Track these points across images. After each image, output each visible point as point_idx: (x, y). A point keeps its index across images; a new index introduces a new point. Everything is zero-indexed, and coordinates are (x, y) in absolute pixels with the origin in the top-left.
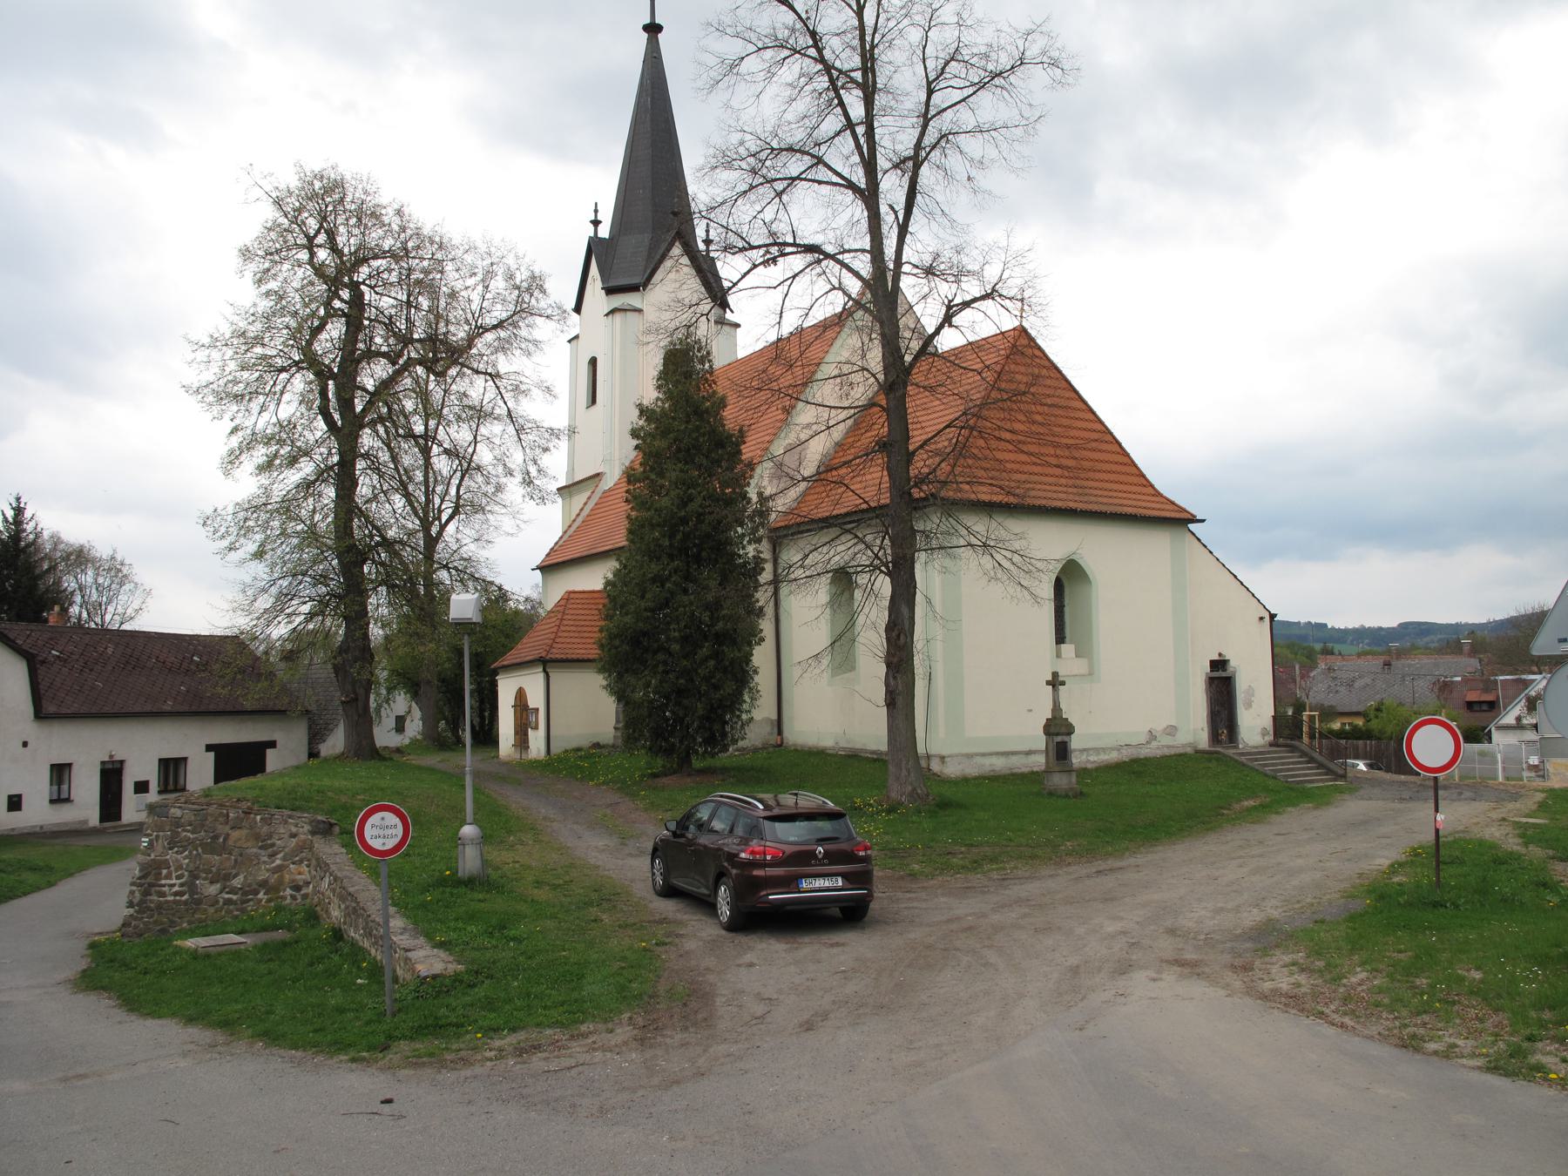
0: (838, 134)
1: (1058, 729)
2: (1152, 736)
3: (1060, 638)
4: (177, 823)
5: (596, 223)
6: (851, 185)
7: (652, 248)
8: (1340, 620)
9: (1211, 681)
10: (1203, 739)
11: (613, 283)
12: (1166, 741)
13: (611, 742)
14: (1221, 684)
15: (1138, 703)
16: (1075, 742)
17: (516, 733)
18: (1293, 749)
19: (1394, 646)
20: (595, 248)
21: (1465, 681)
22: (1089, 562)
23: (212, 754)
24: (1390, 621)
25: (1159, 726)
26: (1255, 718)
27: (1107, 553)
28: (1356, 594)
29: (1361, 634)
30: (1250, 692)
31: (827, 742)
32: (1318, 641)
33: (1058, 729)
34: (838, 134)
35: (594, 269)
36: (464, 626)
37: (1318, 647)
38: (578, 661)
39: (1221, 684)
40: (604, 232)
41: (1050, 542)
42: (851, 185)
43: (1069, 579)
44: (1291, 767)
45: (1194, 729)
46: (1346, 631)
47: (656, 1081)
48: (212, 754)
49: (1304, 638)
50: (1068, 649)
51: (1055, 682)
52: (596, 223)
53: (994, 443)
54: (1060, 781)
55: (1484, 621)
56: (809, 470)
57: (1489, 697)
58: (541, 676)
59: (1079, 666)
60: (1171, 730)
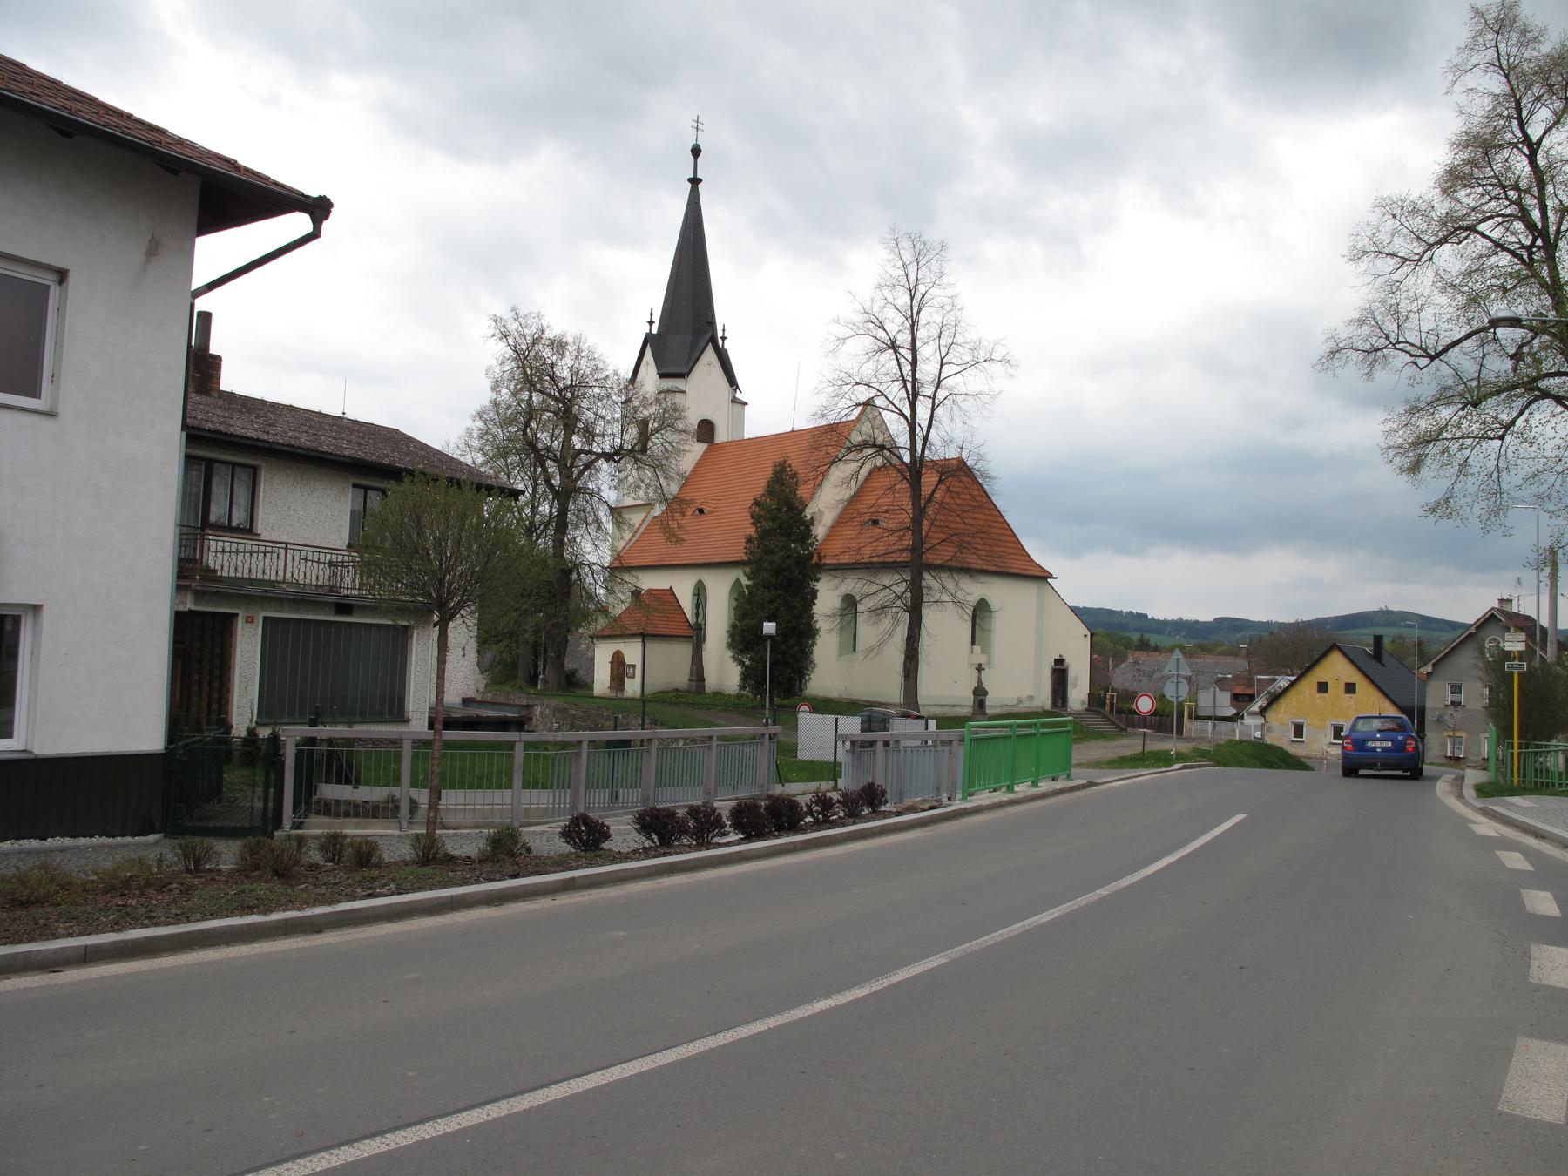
1: (980, 692)
2: (1020, 701)
3: (973, 643)
4: (574, 717)
5: (651, 323)
6: (902, 414)
7: (693, 348)
8: (1161, 610)
9: (1054, 671)
11: (663, 371)
12: (1027, 704)
13: (685, 687)
14: (1060, 674)
15: (1018, 682)
17: (612, 679)
18: (1098, 713)
19: (1206, 639)
20: (648, 340)
21: (1235, 678)
22: (994, 603)
24: (1206, 615)
25: (1024, 695)
26: (1078, 694)
28: (1177, 587)
29: (1179, 626)
30: (1076, 679)
31: (834, 695)
32: (1136, 630)
33: (980, 692)
35: (649, 355)
36: (770, 637)
37: (1135, 637)
39: (1060, 674)
40: (655, 331)
41: (974, 590)
42: (902, 414)
43: (980, 611)
44: (1096, 722)
45: (1043, 697)
46: (1165, 623)
49: (1124, 627)
50: (977, 648)
52: (651, 323)
53: (944, 521)
55: (1292, 620)
56: (828, 596)
57: (1249, 691)
58: (640, 645)
60: (1031, 698)
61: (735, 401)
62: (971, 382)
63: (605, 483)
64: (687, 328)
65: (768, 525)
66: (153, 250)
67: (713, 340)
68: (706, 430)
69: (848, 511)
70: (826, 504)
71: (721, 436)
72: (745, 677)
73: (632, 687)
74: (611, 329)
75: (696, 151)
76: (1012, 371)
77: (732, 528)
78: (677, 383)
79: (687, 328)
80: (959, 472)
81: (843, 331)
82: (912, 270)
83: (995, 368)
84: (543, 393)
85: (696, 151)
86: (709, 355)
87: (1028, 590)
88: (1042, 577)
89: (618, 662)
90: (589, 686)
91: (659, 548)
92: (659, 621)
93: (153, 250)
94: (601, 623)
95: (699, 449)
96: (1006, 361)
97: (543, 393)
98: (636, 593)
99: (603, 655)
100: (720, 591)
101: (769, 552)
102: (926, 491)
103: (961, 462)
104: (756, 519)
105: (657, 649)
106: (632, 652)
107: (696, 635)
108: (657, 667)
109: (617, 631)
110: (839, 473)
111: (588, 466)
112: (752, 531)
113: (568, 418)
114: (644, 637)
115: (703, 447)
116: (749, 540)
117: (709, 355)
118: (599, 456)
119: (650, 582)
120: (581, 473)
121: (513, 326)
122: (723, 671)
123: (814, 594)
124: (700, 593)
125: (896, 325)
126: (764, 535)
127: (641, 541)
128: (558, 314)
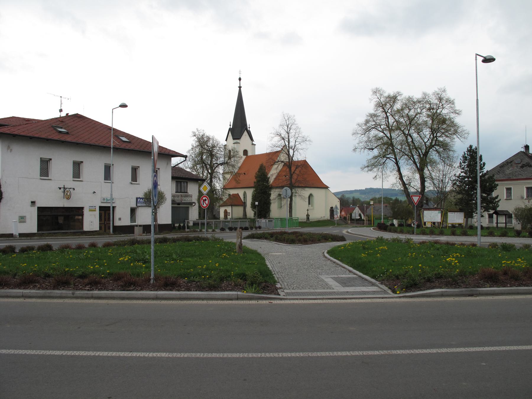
0: (112, 195)
1: (308, 216)
3: (309, 204)
10: (329, 218)
15: (320, 212)
16: (310, 218)
20: (230, 130)
23: (523, 150)
26: (337, 216)
27: (315, 192)
33: (308, 216)
34: (112, 195)
35: (230, 134)
38: (48, 140)
39: (332, 211)
43: (311, 196)
47: (175, 161)
48: (523, 150)
51: (308, 210)
54: (308, 222)
56: (274, 194)
59: (312, 208)
60: (324, 217)
61: (253, 144)
62: (303, 145)
63: (220, 170)
64: (239, 127)
65: (259, 179)
66: (167, 164)
67: (246, 129)
68: (245, 152)
69: (279, 175)
70: (273, 173)
71: (250, 154)
72: (255, 214)
73: (229, 217)
74: (219, 134)
75: (240, 79)
76: (311, 143)
77: (251, 178)
78: (238, 141)
79: (239, 127)
80: (304, 164)
81: (273, 136)
82: (287, 121)
83: (308, 142)
84: (205, 148)
85: (240, 79)
86: (246, 133)
87: (323, 191)
88: (326, 187)
89: (226, 212)
90: (219, 218)
91: (234, 184)
92: (235, 201)
93: (167, 164)
94: (221, 202)
95: (244, 157)
96: (309, 141)
97: (205, 148)
98: (230, 195)
99: (222, 210)
100: (250, 193)
101: (259, 185)
102: (293, 171)
103: (305, 162)
104: (256, 177)
105: (235, 208)
106: (229, 209)
107: (244, 205)
108: (237, 212)
109: (225, 205)
110: (275, 166)
111: (217, 166)
112: (255, 180)
113: (211, 155)
114: (232, 206)
115: (245, 156)
116: (255, 183)
117: (246, 133)
118: (219, 165)
119: (233, 192)
120: (215, 168)
121: (197, 133)
122: (250, 213)
123: (270, 194)
124: (245, 194)
125: (284, 134)
126: (258, 181)
127: (230, 182)
128: (209, 132)
